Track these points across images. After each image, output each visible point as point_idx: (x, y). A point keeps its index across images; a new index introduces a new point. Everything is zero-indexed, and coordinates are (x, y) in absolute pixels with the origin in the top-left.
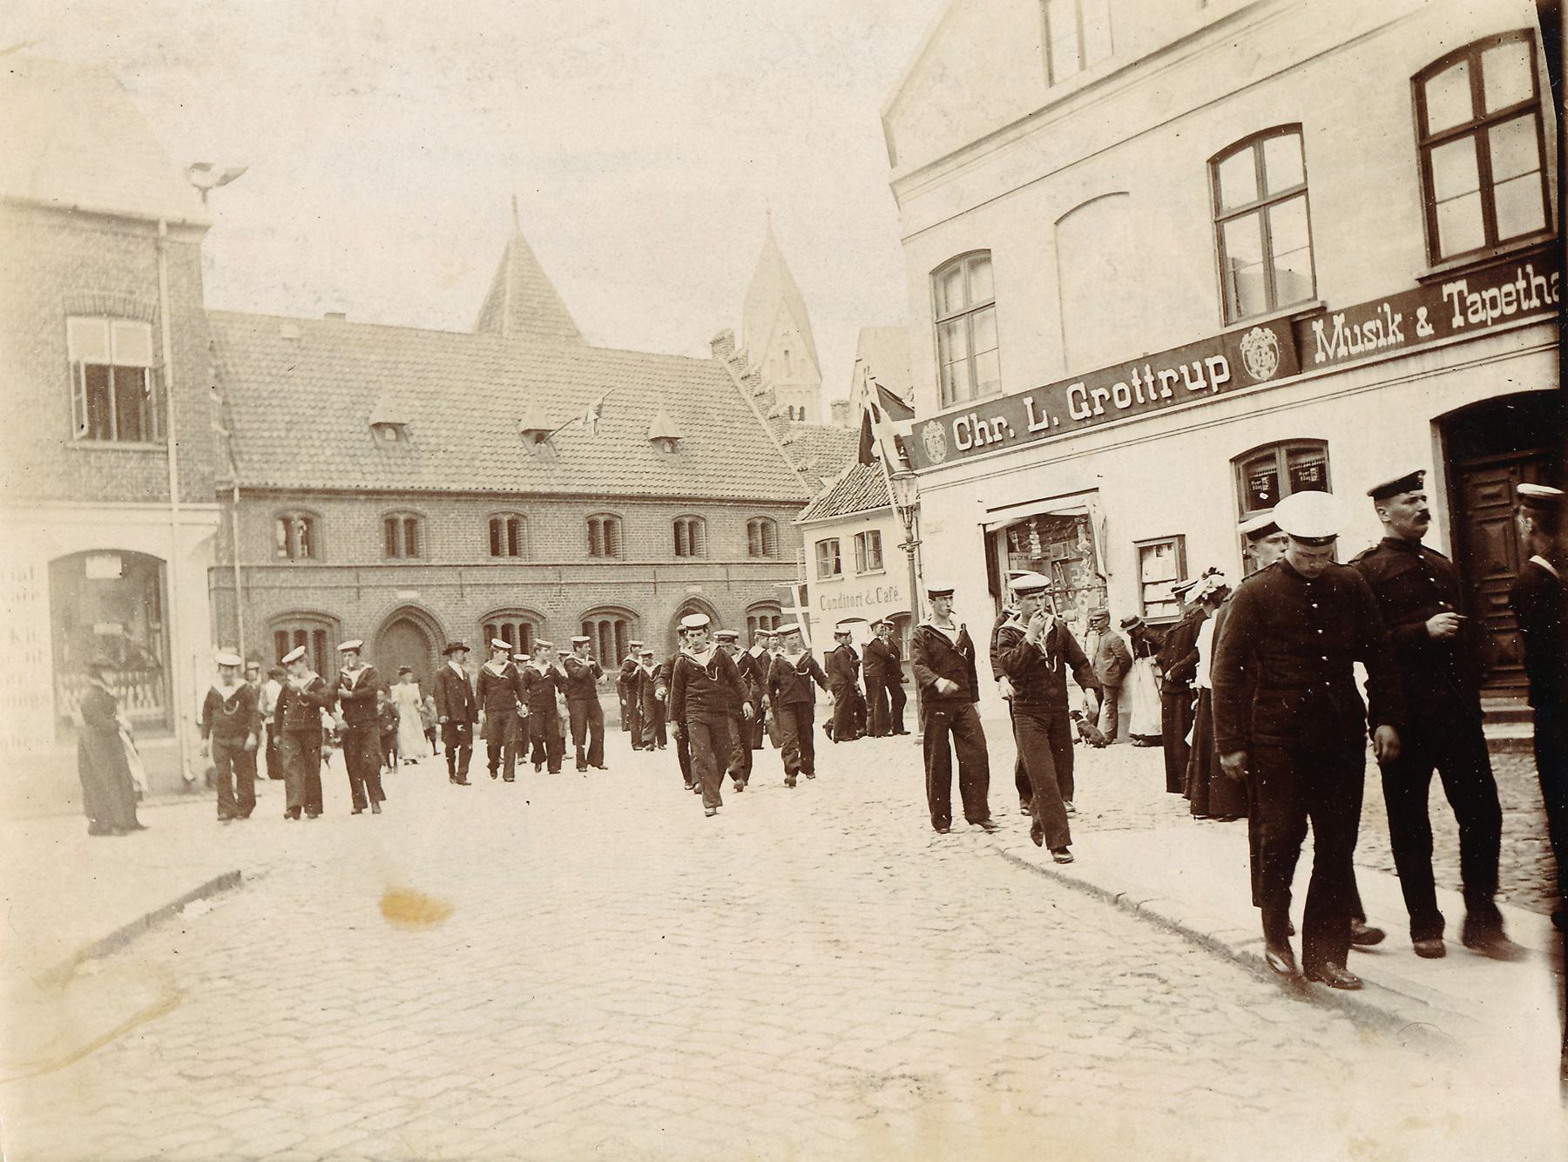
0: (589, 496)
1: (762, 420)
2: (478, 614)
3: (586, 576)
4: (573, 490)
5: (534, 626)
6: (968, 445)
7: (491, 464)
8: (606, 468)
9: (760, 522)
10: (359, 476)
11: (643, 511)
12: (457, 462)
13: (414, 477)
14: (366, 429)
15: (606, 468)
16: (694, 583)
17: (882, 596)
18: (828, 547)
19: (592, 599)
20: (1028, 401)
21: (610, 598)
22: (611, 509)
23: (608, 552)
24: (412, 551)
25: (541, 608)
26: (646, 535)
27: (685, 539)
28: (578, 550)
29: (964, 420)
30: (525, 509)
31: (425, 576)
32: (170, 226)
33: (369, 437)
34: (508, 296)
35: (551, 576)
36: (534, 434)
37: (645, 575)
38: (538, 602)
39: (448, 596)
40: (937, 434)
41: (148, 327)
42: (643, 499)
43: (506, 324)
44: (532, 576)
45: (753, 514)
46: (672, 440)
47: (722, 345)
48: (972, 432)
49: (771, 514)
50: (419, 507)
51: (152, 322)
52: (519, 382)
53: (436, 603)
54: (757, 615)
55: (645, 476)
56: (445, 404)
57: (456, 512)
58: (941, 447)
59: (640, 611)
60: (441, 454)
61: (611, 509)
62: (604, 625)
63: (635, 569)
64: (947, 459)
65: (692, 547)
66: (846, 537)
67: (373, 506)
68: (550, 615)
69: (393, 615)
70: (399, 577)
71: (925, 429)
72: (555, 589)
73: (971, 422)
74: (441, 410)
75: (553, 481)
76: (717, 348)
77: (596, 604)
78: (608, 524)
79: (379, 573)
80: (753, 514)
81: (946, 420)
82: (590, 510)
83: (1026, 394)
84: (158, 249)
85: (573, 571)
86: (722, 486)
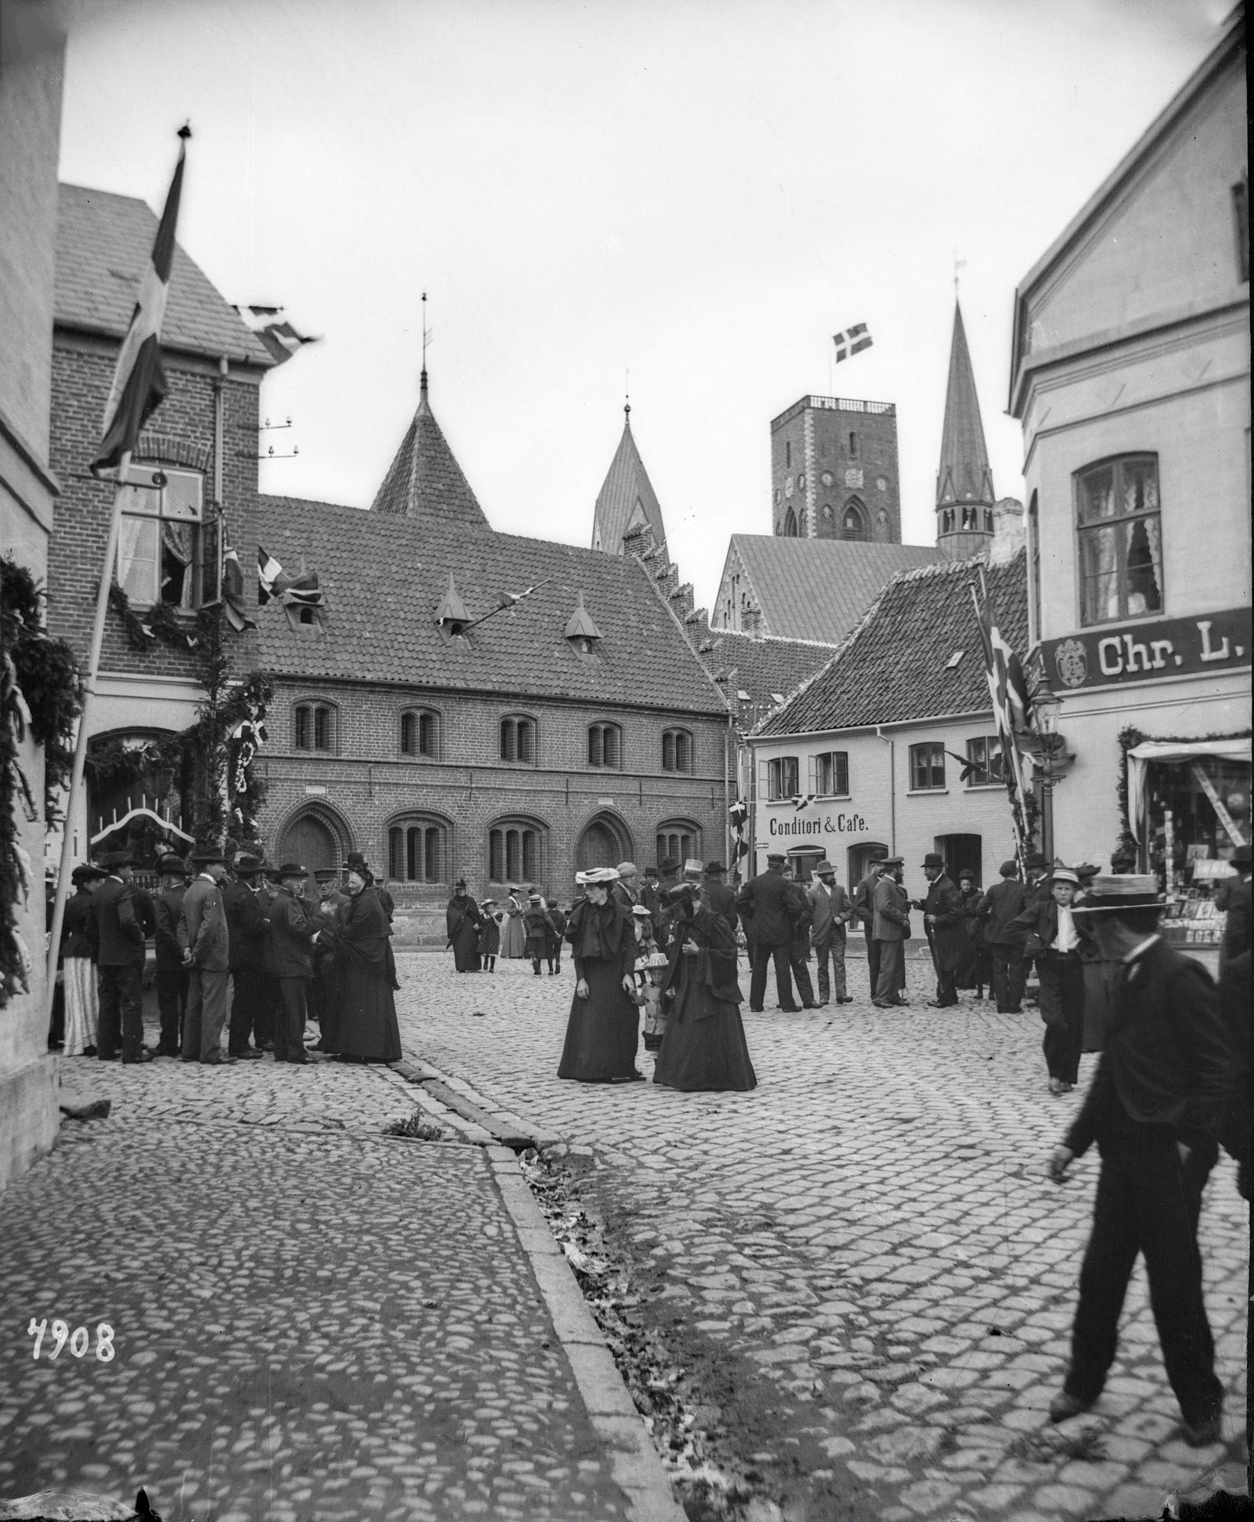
0: (507, 695)
1: (678, 624)
2: (384, 816)
3: (495, 781)
4: (489, 687)
5: (441, 831)
6: (1116, 670)
7: (407, 654)
8: (523, 666)
9: (675, 733)
10: (273, 659)
11: (559, 714)
12: (371, 650)
13: (329, 664)
14: (280, 609)
15: (523, 666)
16: (607, 795)
17: (844, 823)
18: (785, 771)
19: (502, 806)
20: (1204, 626)
21: (520, 805)
22: (526, 710)
23: (424, 750)
24: (322, 744)
25: (452, 813)
26: (561, 739)
27: (602, 745)
28: (489, 754)
29: (1115, 641)
30: (438, 704)
31: (332, 772)
32: (234, 364)
33: (283, 617)
34: (413, 476)
35: (462, 779)
36: (450, 625)
37: (557, 784)
38: (447, 806)
39: (357, 794)
40: (1076, 655)
41: (200, 477)
42: (639, 709)
43: (411, 505)
44: (440, 778)
45: (669, 724)
46: (590, 640)
47: (636, 542)
48: (1125, 655)
49: (688, 726)
50: (331, 696)
51: (205, 472)
52: (433, 568)
53: (343, 802)
54: (667, 833)
55: (563, 677)
56: (358, 586)
57: (367, 703)
58: (1080, 670)
59: (550, 822)
60: (355, 641)
61: (526, 710)
62: (511, 834)
63: (548, 777)
64: (1084, 684)
65: (520, 752)
66: (807, 757)
67: (580, 714)
68: (458, 820)
69: (299, 811)
70: (307, 771)
71: (1060, 648)
72: (465, 794)
73: (1124, 645)
74: (355, 593)
75: (468, 676)
76: (632, 543)
77: (506, 811)
78: (522, 726)
79: (287, 766)
80: (669, 724)
81: (1090, 641)
82: (505, 709)
83: (1202, 618)
84: (216, 389)
85: (485, 774)
86: (639, 692)
